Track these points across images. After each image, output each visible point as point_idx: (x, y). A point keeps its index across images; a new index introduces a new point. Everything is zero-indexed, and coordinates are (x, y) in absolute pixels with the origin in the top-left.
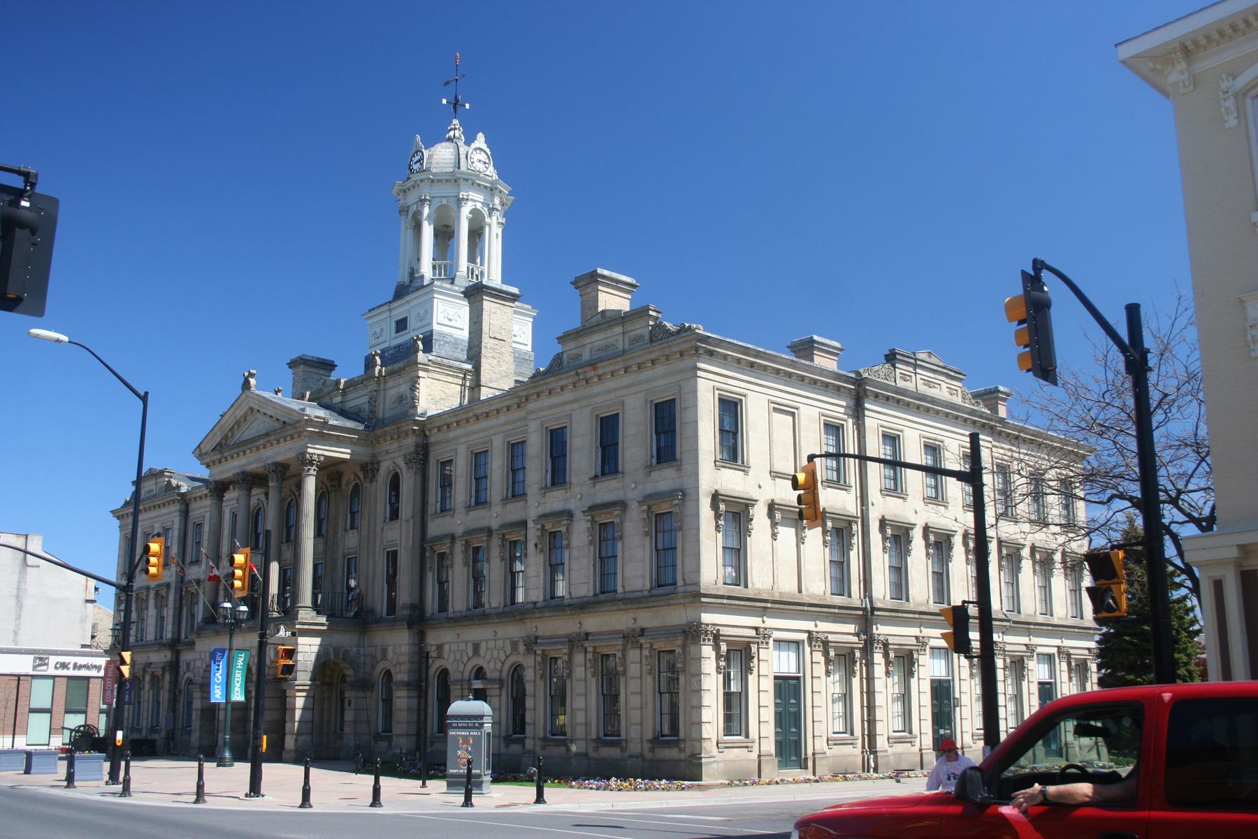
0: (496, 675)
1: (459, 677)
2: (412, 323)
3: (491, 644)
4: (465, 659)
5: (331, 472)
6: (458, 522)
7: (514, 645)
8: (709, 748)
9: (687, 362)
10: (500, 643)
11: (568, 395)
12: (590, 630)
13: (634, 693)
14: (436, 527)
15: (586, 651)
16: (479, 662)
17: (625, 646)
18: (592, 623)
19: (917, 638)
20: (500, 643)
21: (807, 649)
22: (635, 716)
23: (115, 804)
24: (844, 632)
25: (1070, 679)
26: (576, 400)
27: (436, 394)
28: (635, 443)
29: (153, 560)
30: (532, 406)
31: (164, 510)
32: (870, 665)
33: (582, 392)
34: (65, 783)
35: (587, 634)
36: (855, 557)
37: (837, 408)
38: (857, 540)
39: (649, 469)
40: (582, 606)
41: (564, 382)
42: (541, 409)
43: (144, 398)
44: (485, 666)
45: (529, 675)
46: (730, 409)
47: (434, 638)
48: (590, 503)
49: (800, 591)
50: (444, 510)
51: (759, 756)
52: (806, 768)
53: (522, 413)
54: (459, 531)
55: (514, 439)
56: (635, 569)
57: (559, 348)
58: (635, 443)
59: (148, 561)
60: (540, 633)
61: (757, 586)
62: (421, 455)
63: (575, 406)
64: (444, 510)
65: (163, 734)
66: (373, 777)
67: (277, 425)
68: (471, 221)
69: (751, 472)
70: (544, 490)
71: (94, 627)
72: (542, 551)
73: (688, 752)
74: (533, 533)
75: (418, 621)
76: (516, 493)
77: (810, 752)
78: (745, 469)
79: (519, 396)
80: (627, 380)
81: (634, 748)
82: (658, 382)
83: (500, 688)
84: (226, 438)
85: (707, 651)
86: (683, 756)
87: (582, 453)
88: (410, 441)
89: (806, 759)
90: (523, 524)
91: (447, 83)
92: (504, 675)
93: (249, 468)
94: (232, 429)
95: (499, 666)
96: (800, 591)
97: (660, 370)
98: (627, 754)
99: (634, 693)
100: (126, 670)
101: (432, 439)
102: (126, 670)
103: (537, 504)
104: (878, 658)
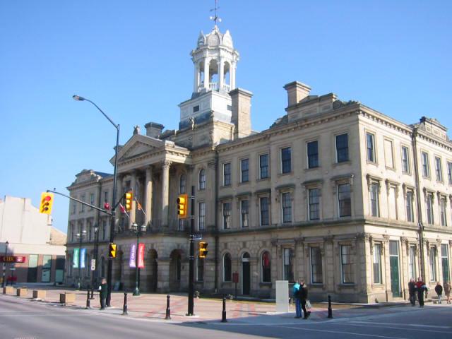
0: (255, 256)
1: (235, 256)
2: (201, 108)
3: (252, 243)
4: (239, 249)
5: (175, 167)
6: (234, 190)
7: (264, 243)
8: (369, 288)
9: (353, 118)
10: (257, 242)
11: (291, 134)
12: (306, 236)
13: (330, 264)
14: (222, 193)
15: (277, 246)
16: (246, 250)
17: (324, 243)
18: (306, 233)
19: (384, 235)
20: (257, 242)
21: (400, 243)
22: (331, 274)
23: (146, 323)
24: (412, 236)
25: (407, 254)
26: (295, 136)
27: (220, 133)
28: (328, 152)
29: (182, 207)
30: (272, 139)
31: (91, 187)
32: (422, 251)
33: (298, 132)
34: (122, 312)
35: (304, 238)
36: (415, 203)
37: (407, 140)
38: (415, 197)
39: (334, 165)
40: (302, 226)
41: (289, 128)
42: (277, 140)
43: (117, 127)
44: (249, 252)
45: (274, 255)
46: (371, 138)
47: (222, 240)
48: (304, 180)
49: (397, 219)
50: (228, 185)
51: (386, 292)
52: (402, 296)
53: (267, 142)
54: (253, 191)
55: (262, 153)
56: (330, 209)
57: (286, 113)
58: (328, 152)
59: (179, 207)
60: (279, 237)
61: (383, 216)
62: (215, 164)
63: (295, 138)
64: (228, 185)
65: (91, 279)
66: (123, 294)
67: (150, 149)
68: (225, 67)
69: (379, 166)
70: (279, 175)
71: (51, 235)
72: (279, 202)
73: (359, 291)
74: (274, 194)
75: (215, 232)
76: (265, 177)
77: (403, 289)
78: (376, 163)
79: (255, 138)
80: (323, 126)
81: (331, 288)
82: (339, 126)
83: (257, 262)
84: (125, 154)
85: (367, 244)
86: (356, 292)
87: (300, 158)
88: (211, 155)
89: (401, 293)
90: (269, 191)
91: (211, 10)
92: (259, 255)
93: (135, 167)
94: (128, 151)
95: (256, 252)
96: (397, 219)
97: (339, 121)
98: (326, 291)
99: (330, 264)
100: (113, 253)
101: (220, 155)
102: (113, 253)
103: (277, 180)
104: (425, 247)
